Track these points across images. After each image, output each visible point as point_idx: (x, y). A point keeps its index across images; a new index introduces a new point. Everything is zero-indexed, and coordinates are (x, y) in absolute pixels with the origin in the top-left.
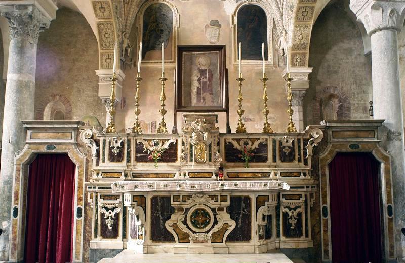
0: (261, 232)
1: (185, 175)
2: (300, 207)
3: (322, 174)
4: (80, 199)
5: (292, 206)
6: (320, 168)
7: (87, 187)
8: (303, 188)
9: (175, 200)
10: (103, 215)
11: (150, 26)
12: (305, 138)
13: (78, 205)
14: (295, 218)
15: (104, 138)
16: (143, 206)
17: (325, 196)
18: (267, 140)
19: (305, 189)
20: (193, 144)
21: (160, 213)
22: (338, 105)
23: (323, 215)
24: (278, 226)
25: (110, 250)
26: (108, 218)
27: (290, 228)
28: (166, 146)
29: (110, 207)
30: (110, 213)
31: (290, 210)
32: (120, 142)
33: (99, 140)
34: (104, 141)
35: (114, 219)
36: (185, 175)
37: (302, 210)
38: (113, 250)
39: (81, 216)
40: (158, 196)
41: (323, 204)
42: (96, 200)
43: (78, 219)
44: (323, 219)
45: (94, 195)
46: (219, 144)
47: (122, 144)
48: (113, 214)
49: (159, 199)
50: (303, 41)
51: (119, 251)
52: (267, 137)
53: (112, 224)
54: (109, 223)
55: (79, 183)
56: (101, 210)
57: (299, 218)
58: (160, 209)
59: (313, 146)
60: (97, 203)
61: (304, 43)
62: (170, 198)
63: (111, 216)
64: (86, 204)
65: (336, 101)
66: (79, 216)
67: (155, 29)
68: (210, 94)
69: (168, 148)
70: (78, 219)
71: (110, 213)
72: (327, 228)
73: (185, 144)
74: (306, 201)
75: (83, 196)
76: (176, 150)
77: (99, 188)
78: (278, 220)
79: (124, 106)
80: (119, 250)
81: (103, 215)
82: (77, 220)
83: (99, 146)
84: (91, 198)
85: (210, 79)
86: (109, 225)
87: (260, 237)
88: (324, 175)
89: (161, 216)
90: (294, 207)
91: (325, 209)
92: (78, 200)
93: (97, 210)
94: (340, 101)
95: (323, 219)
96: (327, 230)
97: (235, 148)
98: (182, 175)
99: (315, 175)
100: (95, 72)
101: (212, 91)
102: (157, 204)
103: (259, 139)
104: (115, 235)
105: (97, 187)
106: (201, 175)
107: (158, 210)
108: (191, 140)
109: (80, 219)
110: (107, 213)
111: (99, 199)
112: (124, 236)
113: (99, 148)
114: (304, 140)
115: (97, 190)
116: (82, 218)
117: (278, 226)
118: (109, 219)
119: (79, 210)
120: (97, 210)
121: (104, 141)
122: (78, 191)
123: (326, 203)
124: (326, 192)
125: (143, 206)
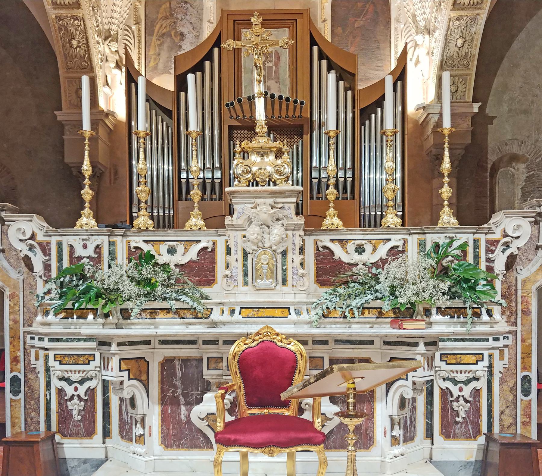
0: (347, 326)
1: (233, 312)
2: (478, 379)
3: (522, 311)
4: (15, 360)
5: (461, 377)
6: (519, 300)
7: (29, 337)
8: (487, 340)
9: (212, 366)
10: (60, 392)
11: (158, 26)
12: (490, 236)
13: (12, 371)
14: (467, 401)
15: (59, 238)
16: (144, 378)
17: (527, 354)
18: (405, 242)
19: (491, 343)
20: (248, 250)
21: (180, 391)
22: (526, 175)
23: (522, 392)
24: (429, 415)
25: (79, 460)
26: (72, 397)
27: (454, 418)
28: (193, 253)
29: (75, 377)
30: (76, 389)
31: (456, 385)
32: (91, 247)
33: (49, 243)
34: (59, 244)
35: (86, 401)
36: (233, 312)
37: (482, 384)
38: (85, 461)
39: (20, 392)
40: (175, 358)
41: (524, 368)
42: (46, 364)
43: (14, 398)
44: (522, 400)
45: (42, 353)
46: (302, 250)
47: (98, 249)
48: (82, 390)
49: (177, 364)
50: (465, 50)
51: (98, 464)
52: (406, 237)
53: (80, 411)
54: (75, 407)
55: (11, 329)
56: (56, 383)
57: (475, 402)
58: (179, 384)
59: (508, 253)
60: (47, 370)
61: (467, 54)
62: (200, 360)
63: (79, 396)
64: (29, 369)
65: (522, 167)
66: (15, 392)
67: (170, 31)
68: (276, 82)
69: (195, 258)
70: (14, 398)
71: (76, 389)
72: (530, 417)
73: (233, 251)
74: (490, 367)
75: (21, 354)
76: (213, 262)
77: (50, 340)
78: (430, 402)
79: (116, 179)
80: (96, 460)
81: (60, 392)
82: (11, 399)
83: (50, 255)
84: (37, 358)
85: (276, 65)
86: (75, 412)
87: (395, 441)
88: (526, 312)
89: (181, 398)
90: (465, 379)
91: (526, 379)
92: (11, 363)
93: (48, 384)
94: (529, 168)
95: (522, 400)
96: (530, 422)
97: (336, 257)
98: (226, 312)
99: (508, 313)
100: (56, 116)
101: (278, 78)
102: (175, 375)
103: (390, 240)
104: (90, 433)
105: (46, 339)
106: (267, 313)
107: (175, 386)
108: (244, 242)
109: (18, 397)
110: (69, 390)
111: (51, 362)
112: (107, 434)
113: (50, 259)
114: (488, 242)
115: (46, 344)
116: (22, 396)
117: (429, 415)
118: (76, 400)
119: (15, 380)
120: (48, 384)
121: (59, 244)
122: (11, 343)
123: (529, 369)
124: (530, 346)
125: (144, 378)
